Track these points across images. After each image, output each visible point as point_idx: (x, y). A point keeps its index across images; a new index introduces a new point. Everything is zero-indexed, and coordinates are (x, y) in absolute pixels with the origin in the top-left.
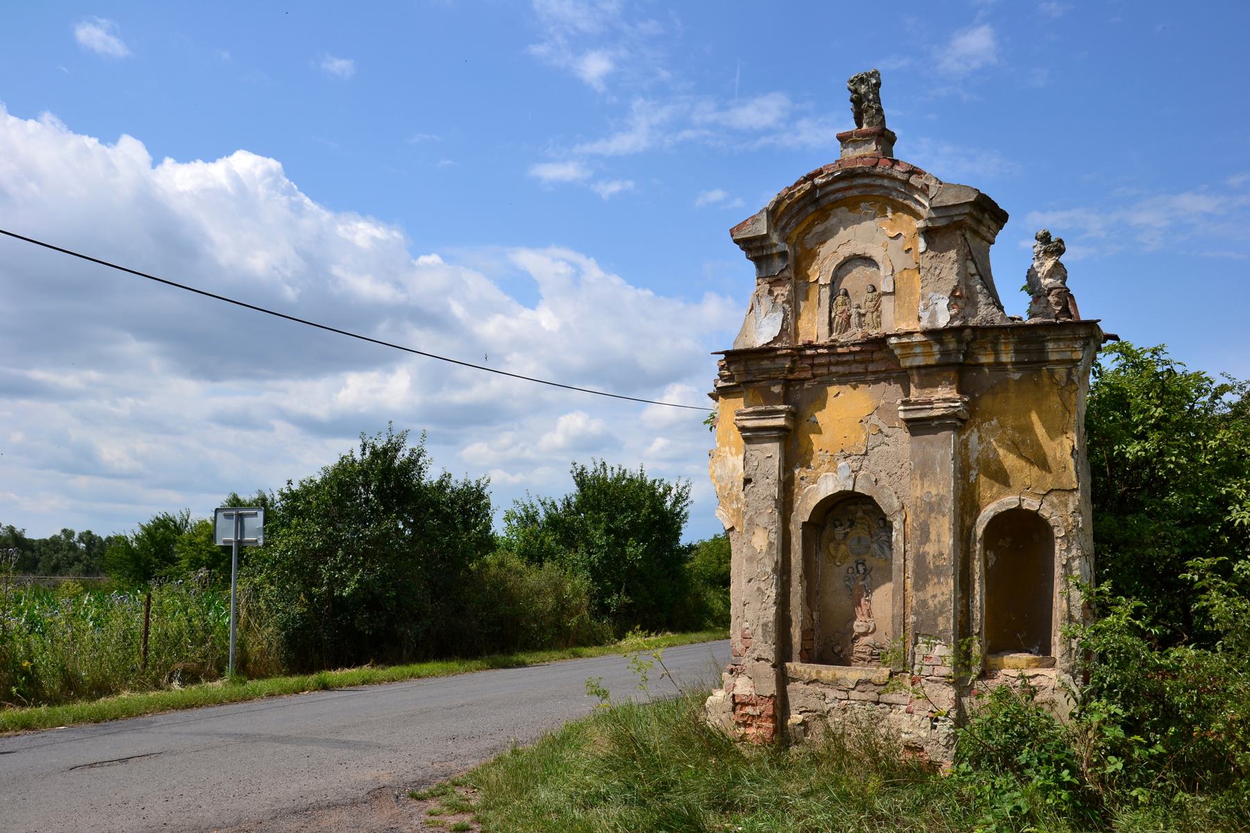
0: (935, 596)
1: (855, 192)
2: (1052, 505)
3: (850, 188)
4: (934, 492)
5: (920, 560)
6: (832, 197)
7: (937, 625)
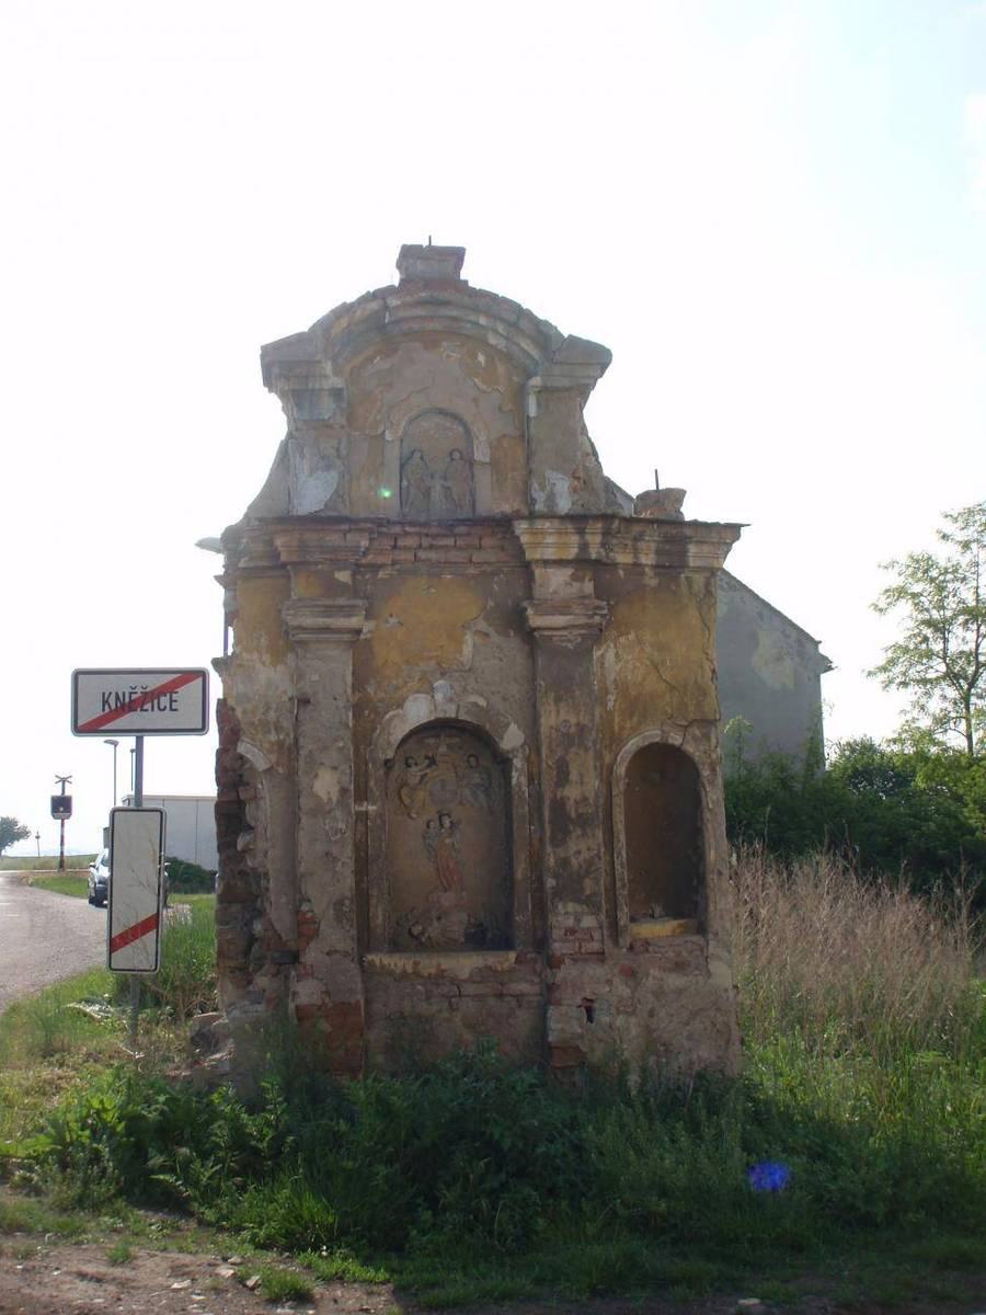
0: (579, 852)
1: (431, 326)
2: (695, 738)
3: (431, 318)
4: (573, 720)
5: (559, 805)
6: (405, 326)
7: (583, 889)
